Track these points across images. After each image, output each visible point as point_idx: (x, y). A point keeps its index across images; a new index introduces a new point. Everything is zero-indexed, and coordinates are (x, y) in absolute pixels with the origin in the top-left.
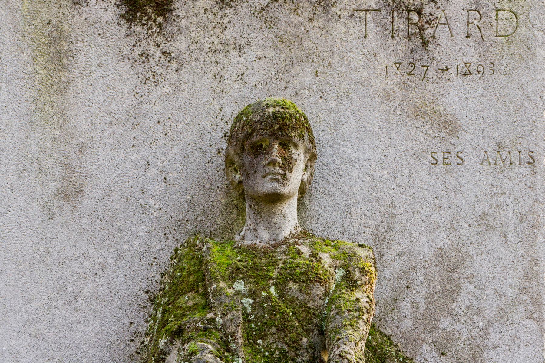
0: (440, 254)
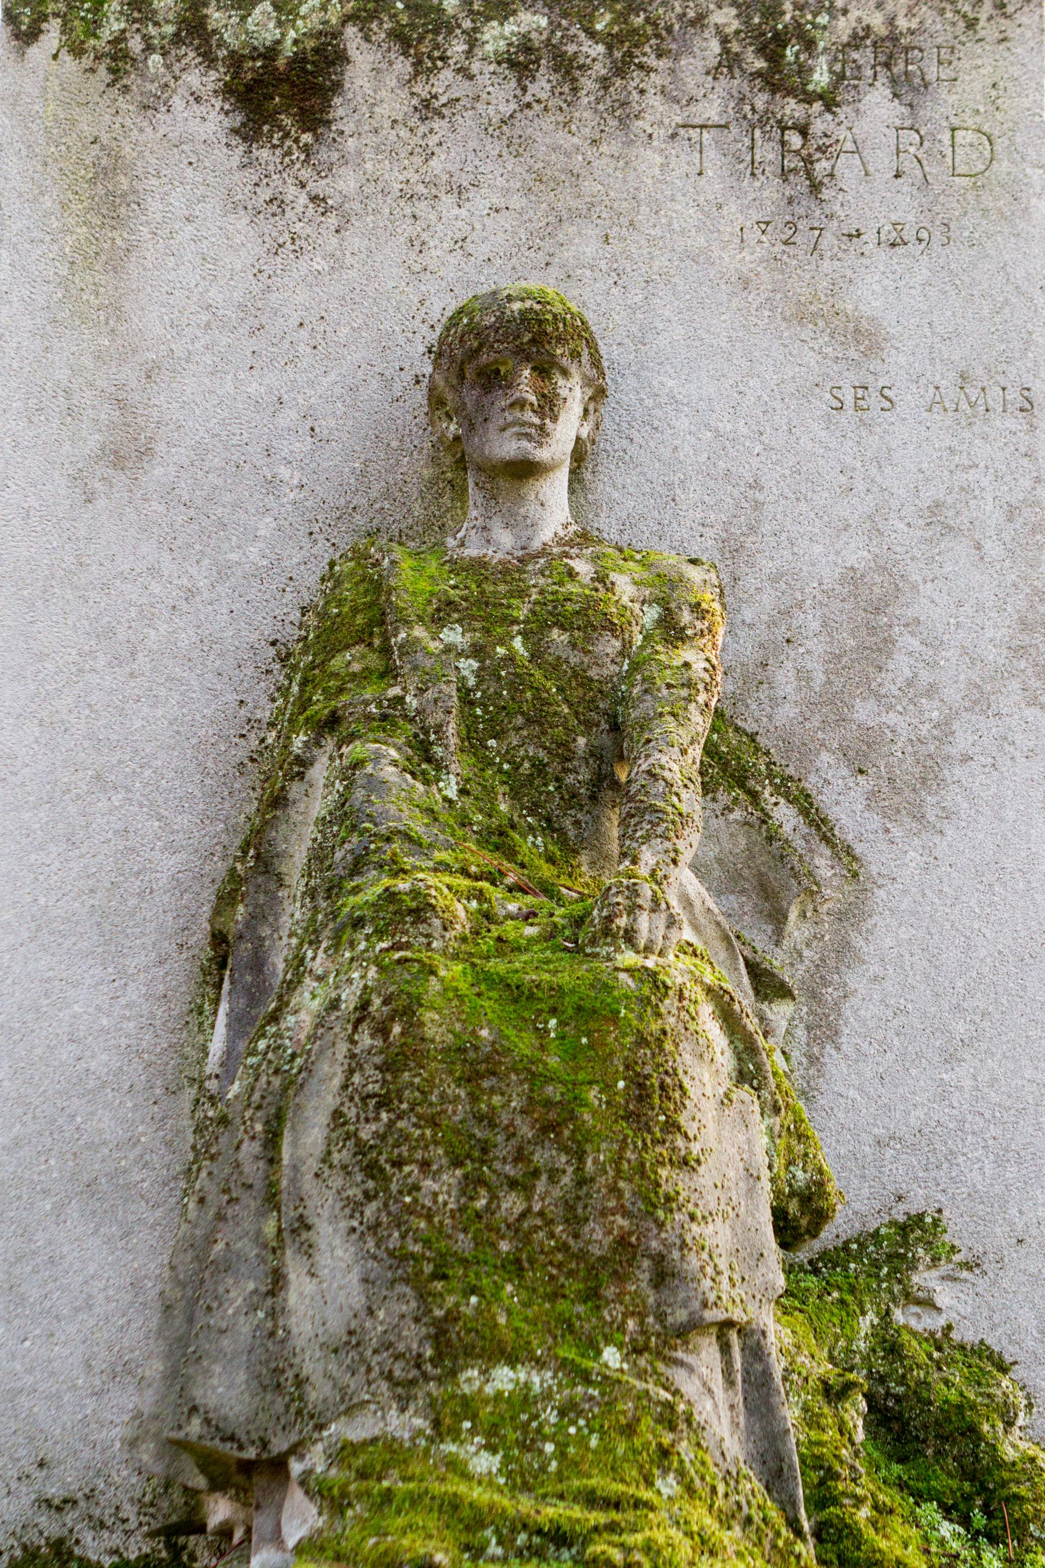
0: (852, 578)
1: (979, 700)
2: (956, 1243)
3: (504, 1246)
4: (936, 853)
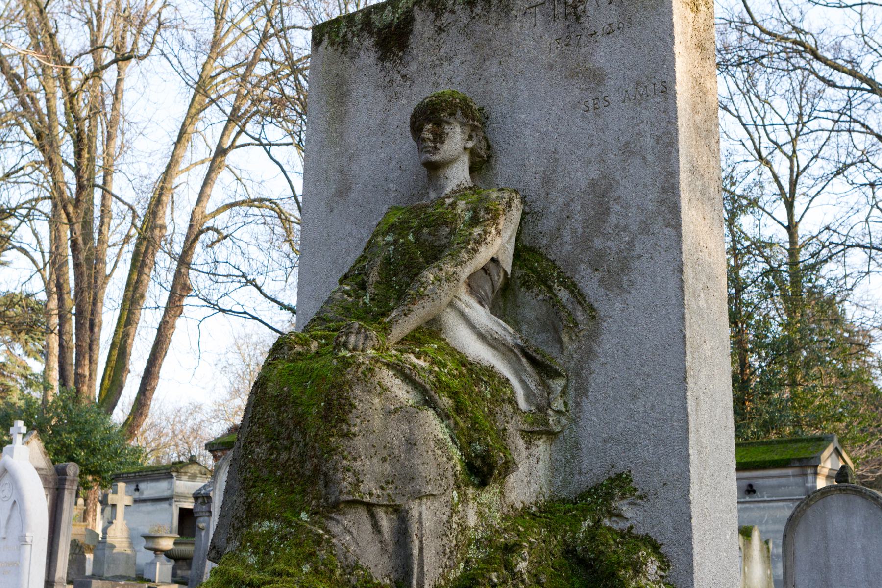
0: (593, 184)
1: (645, 229)
2: (637, 486)
3: (279, 473)
4: (628, 302)
